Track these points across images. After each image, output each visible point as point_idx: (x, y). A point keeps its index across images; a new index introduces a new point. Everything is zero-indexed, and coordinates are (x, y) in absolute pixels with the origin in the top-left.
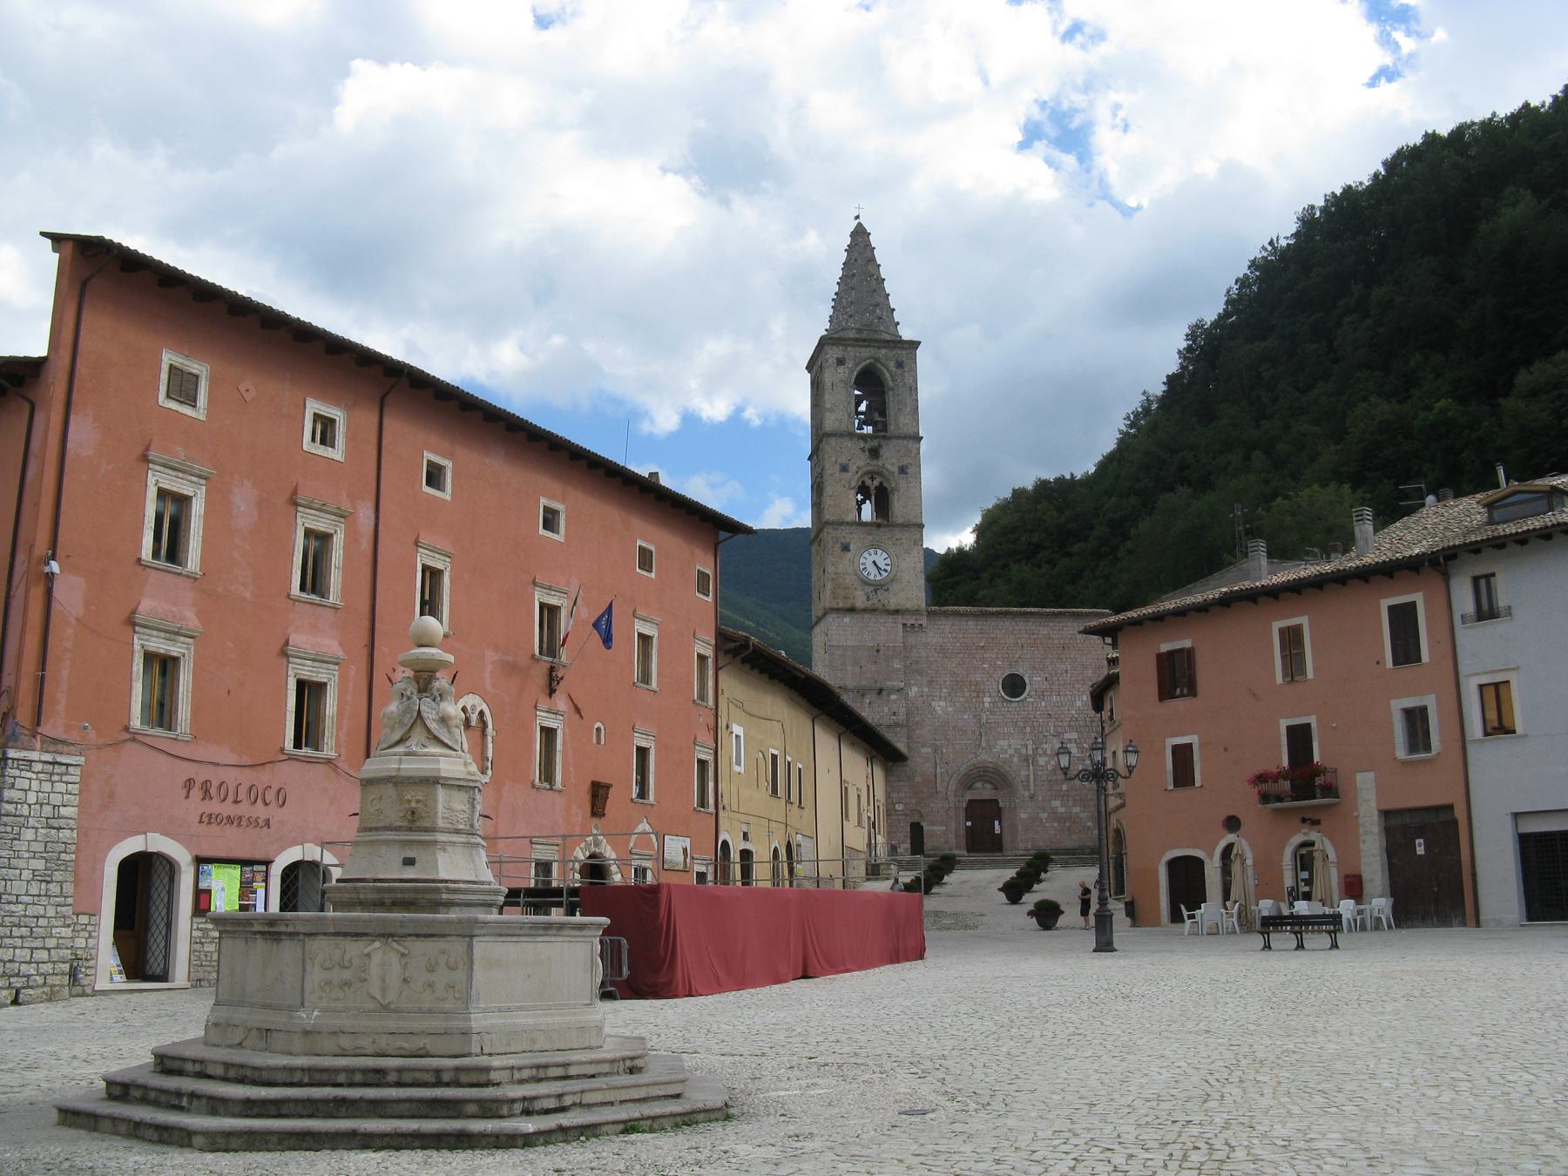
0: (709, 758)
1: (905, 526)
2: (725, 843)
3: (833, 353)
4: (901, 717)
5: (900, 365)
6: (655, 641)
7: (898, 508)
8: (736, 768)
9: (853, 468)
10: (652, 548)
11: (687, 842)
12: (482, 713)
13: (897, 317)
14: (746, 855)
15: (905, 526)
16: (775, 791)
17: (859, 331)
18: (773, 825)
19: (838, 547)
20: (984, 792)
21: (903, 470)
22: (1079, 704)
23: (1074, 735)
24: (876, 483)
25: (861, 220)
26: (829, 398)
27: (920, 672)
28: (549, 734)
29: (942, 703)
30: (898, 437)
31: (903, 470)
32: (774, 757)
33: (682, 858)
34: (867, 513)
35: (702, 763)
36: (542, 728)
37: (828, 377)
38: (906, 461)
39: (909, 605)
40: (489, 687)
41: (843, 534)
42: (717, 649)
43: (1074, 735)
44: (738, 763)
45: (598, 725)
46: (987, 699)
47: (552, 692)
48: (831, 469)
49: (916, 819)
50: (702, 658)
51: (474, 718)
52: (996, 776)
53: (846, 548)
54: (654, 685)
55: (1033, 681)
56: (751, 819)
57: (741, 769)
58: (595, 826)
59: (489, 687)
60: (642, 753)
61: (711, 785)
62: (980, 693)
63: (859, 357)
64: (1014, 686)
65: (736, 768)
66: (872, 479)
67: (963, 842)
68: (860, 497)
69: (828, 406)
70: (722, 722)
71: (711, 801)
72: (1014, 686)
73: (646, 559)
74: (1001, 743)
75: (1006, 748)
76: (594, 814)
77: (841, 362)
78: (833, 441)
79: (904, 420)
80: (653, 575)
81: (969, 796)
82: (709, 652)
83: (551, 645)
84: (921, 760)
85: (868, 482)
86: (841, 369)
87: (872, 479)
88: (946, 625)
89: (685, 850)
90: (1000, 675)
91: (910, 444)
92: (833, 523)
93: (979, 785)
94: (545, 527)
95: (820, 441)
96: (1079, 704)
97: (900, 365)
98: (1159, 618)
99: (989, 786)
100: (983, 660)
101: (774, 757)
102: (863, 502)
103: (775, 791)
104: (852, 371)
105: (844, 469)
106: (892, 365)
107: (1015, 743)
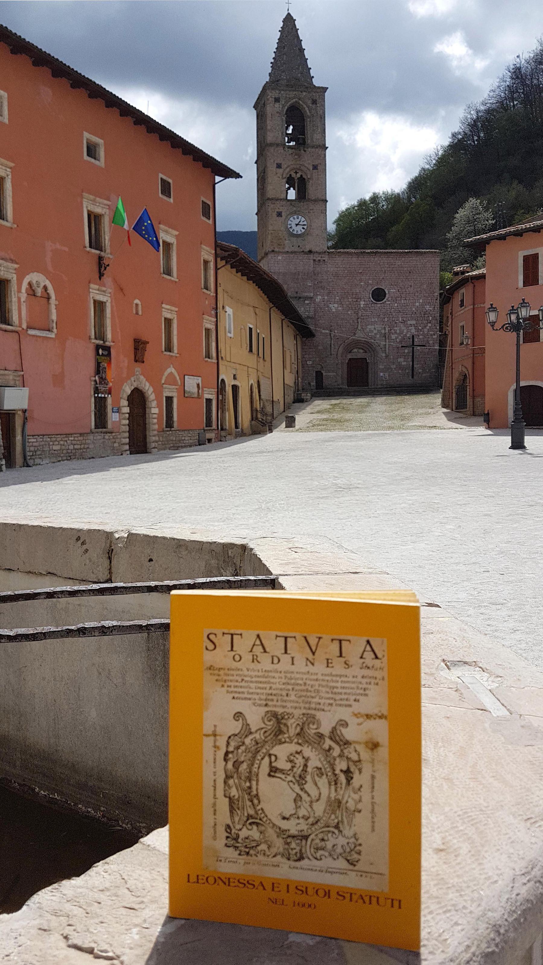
0: (212, 327)
1: (316, 201)
2: (223, 380)
3: (272, 95)
4: (312, 314)
5: (314, 102)
6: (175, 248)
7: (311, 192)
8: (229, 335)
9: (284, 166)
10: (170, 181)
11: (199, 380)
12: (45, 288)
13: (312, 73)
14: (235, 388)
15: (316, 201)
16: (251, 350)
17: (288, 81)
18: (250, 370)
19: (275, 214)
20: (358, 353)
21: (315, 167)
22: (417, 304)
23: (414, 322)
24: (298, 176)
25: (290, 12)
26: (269, 124)
27: (323, 288)
28: (100, 306)
29: (336, 305)
30: (313, 147)
31: (315, 167)
32: (251, 329)
33: (196, 390)
34: (292, 194)
35: (208, 331)
36: (95, 301)
37: (269, 109)
38: (316, 163)
39: (317, 249)
40: (50, 268)
41: (279, 206)
42: (216, 256)
43: (414, 322)
44: (230, 332)
45: (137, 301)
46: (362, 303)
47: (101, 275)
48: (271, 168)
49: (319, 368)
50: (206, 262)
51: (39, 292)
52: (368, 347)
53: (279, 214)
54: (174, 278)
55: (390, 292)
56: (238, 366)
57: (232, 335)
58: (138, 368)
59: (50, 268)
60: (168, 322)
61: (214, 344)
62: (358, 299)
63: (290, 97)
64: (379, 295)
65: (229, 335)
66: (296, 173)
67: (345, 381)
68: (287, 186)
69: (269, 128)
70: (220, 305)
71: (214, 355)
72: (379, 295)
73: (166, 188)
74: (369, 327)
75: (373, 329)
76: (136, 361)
77: (277, 100)
78: (272, 149)
79: (317, 136)
80: (171, 200)
81: (349, 356)
82: (211, 258)
83: (96, 242)
84: (322, 334)
85: (294, 175)
86: (277, 105)
87: (296, 173)
88: (339, 260)
89: (198, 385)
90: (370, 289)
91: (320, 151)
92: (272, 199)
93: (355, 350)
94: (88, 155)
95: (264, 150)
96: (417, 304)
97: (314, 102)
98: (519, 234)
99: (361, 351)
100: (361, 280)
101: (251, 329)
102: (289, 188)
103: (251, 350)
104: (284, 106)
105: (279, 166)
106: (309, 102)
107: (378, 327)
